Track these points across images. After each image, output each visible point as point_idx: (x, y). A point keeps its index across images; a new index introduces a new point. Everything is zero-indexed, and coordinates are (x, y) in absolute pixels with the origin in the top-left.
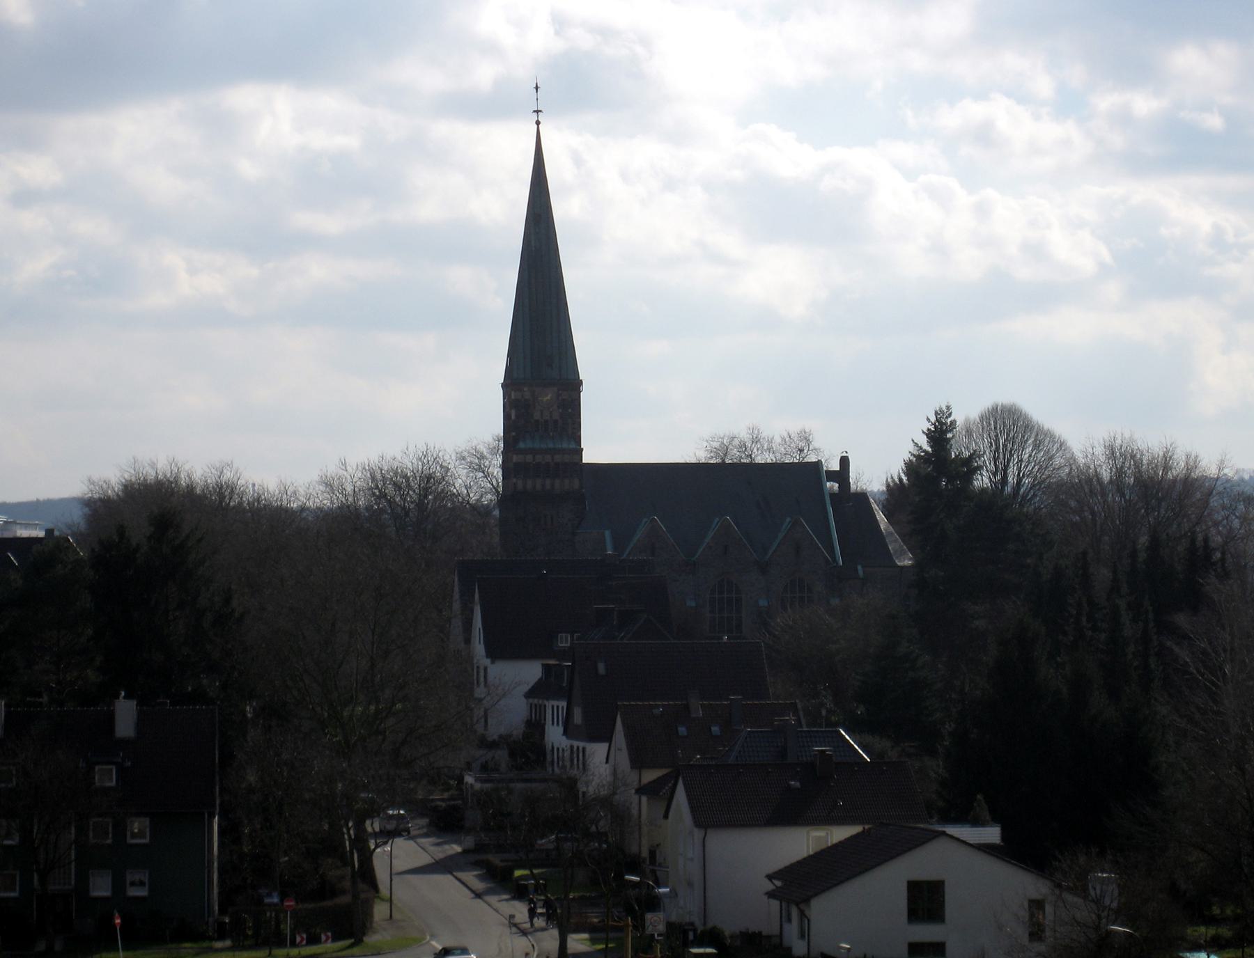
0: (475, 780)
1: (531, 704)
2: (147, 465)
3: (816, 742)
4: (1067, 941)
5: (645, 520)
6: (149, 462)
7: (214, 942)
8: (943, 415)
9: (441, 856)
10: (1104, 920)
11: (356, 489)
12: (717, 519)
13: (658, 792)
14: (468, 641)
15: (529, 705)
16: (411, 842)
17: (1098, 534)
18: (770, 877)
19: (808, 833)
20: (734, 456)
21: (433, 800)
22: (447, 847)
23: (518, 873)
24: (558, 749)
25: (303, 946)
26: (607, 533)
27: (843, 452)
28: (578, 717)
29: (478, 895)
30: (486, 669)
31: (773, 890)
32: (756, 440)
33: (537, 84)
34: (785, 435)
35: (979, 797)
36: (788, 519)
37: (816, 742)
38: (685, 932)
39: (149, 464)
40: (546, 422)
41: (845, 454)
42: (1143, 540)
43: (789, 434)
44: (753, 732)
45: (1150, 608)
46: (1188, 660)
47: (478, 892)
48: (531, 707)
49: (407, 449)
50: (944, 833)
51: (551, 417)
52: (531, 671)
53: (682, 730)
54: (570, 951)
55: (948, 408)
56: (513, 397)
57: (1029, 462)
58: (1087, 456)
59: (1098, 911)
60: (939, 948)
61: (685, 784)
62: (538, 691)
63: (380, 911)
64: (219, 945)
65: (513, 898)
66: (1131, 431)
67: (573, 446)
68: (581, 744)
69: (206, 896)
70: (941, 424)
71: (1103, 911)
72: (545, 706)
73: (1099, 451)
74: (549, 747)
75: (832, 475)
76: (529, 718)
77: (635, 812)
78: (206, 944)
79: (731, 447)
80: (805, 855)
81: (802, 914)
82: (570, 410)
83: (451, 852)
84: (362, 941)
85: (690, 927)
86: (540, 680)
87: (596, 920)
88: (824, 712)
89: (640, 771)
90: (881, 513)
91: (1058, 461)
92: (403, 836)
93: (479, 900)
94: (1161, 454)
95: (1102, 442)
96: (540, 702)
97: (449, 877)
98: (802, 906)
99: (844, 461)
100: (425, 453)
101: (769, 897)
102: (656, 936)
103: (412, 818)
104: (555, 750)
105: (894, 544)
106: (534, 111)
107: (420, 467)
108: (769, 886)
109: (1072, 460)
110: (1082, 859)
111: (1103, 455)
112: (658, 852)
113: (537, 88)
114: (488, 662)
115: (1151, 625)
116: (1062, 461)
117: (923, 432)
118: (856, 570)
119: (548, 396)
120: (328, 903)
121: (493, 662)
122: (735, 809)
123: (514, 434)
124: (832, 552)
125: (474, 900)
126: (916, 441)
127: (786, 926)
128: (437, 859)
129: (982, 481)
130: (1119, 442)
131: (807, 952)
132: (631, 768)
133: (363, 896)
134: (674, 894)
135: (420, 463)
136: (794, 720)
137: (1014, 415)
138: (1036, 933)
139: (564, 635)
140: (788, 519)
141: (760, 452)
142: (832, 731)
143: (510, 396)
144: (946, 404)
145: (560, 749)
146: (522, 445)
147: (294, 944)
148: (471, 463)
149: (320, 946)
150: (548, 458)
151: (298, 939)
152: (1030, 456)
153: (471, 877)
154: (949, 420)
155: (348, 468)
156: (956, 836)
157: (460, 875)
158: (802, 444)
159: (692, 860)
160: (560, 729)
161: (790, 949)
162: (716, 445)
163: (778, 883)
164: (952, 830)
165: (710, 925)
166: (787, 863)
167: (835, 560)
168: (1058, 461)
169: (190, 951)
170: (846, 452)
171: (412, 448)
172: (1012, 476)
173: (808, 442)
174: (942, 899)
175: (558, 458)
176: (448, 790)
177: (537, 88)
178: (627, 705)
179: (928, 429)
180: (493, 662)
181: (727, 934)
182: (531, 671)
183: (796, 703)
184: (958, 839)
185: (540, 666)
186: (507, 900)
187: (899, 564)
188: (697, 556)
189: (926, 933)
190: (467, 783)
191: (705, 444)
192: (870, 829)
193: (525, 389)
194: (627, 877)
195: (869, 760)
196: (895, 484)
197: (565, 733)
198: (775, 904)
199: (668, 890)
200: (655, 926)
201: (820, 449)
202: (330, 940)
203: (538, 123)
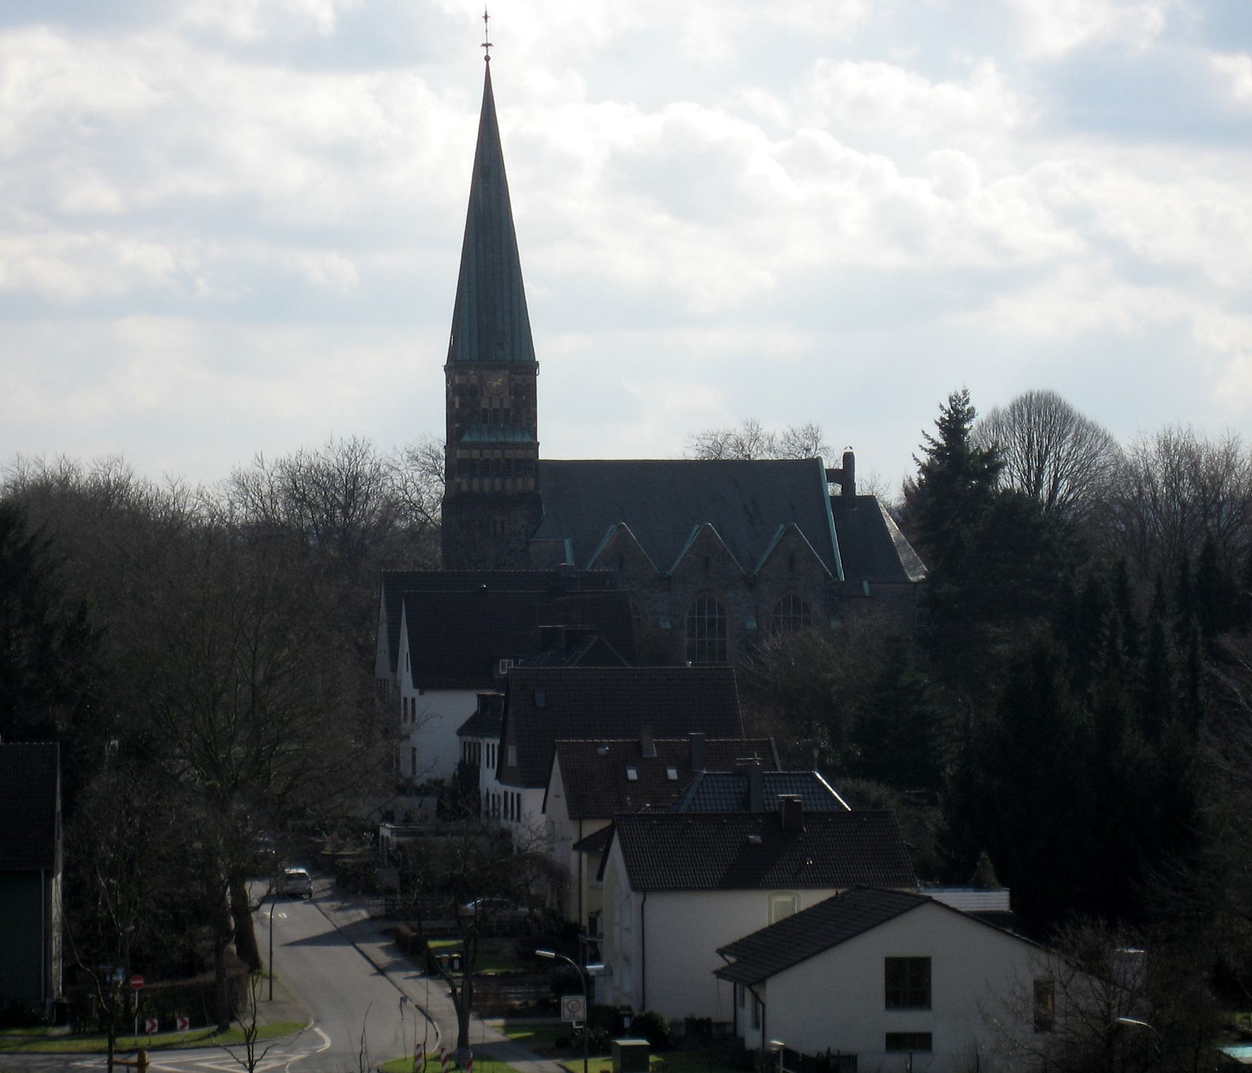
0: (392, 834)
1: (465, 743)
2: (32, 462)
3: (786, 787)
4: (1069, 1035)
5: (612, 527)
6: (36, 460)
7: (50, 1028)
8: (959, 401)
9: (344, 923)
10: (1115, 1010)
11: (275, 491)
12: (697, 526)
13: (595, 846)
14: (394, 668)
15: (463, 743)
16: (312, 907)
17: (1148, 545)
18: (722, 952)
19: (770, 900)
20: (730, 454)
21: (343, 856)
22: (352, 912)
23: (433, 944)
24: (493, 796)
25: (153, 1034)
26: (567, 542)
27: (846, 448)
28: (512, 758)
29: (381, 971)
30: (413, 700)
31: (724, 969)
32: (755, 438)
33: (486, 13)
34: (788, 431)
35: (984, 855)
36: (782, 526)
37: (786, 787)
38: (619, 1019)
39: (35, 462)
40: (496, 410)
41: (849, 450)
42: (1197, 552)
43: (792, 431)
44: (709, 775)
45: (1199, 629)
46: (1236, 690)
47: (381, 967)
48: (465, 747)
49: (331, 443)
50: (929, 899)
51: (502, 405)
52: (464, 705)
53: (632, 774)
54: (471, 1042)
55: (965, 393)
56: (457, 382)
57: (1067, 461)
58: (1138, 453)
59: (1108, 998)
60: (921, 1041)
61: (621, 839)
62: (471, 728)
63: (258, 990)
64: (57, 1031)
65: (423, 975)
66: (1189, 424)
67: (527, 439)
68: (516, 790)
69: (43, 972)
70: (957, 412)
71: (1114, 998)
72: (480, 744)
73: (1152, 447)
74: (483, 794)
75: (834, 475)
76: (462, 759)
77: (574, 872)
78: (37, 1031)
79: (726, 446)
80: (766, 925)
81: (756, 997)
82: (524, 398)
83: (358, 919)
84: (229, 1028)
85: (627, 1012)
86: (476, 714)
87: (517, 1003)
88: (816, 753)
89: (581, 824)
90: (891, 519)
91: (1102, 459)
92: (304, 899)
93: (381, 977)
94: (1222, 449)
95: (1155, 436)
96: (475, 740)
97: (352, 948)
98: (755, 988)
99: (849, 458)
100: (352, 447)
101: (718, 977)
102: (574, 1024)
103: (315, 879)
104: (491, 798)
105: (907, 555)
106: (483, 45)
107: (347, 464)
108: (720, 963)
109: (1118, 458)
110: (1087, 933)
111: (1156, 452)
112: (599, 919)
113: (486, 17)
114: (415, 693)
115: (1200, 650)
116: (1107, 458)
117: (936, 422)
118: (861, 586)
119: (497, 381)
120: (190, 981)
121: (421, 693)
122: (831, 857)
123: (457, 425)
124: (833, 566)
125: (376, 977)
126: (926, 433)
127: (740, 1011)
128: (338, 926)
129: (1009, 480)
130: (1175, 436)
131: (761, 1046)
132: (570, 818)
133: (231, 972)
134: (609, 971)
135: (346, 459)
136: (759, 761)
137: (1051, 404)
138: (1042, 1025)
139: (506, 661)
140: (782, 526)
141: (759, 452)
142: (807, 774)
143: (453, 381)
144: (962, 388)
145: (496, 796)
146: (466, 439)
147: (142, 1031)
148: (425, 463)
149: (175, 1034)
150: (498, 453)
151: (148, 1025)
152: (1069, 454)
153: (379, 950)
154: (967, 407)
155: (266, 465)
156: (944, 902)
157: (365, 946)
158: (807, 443)
159: (628, 930)
160: (493, 772)
161: (742, 1040)
162: (709, 443)
163: (732, 960)
164: (938, 895)
165: (649, 1009)
166: (736, 938)
167: (836, 574)
168: (1102, 459)
169: (19, 1039)
170: (851, 448)
171: (337, 442)
172: (1048, 478)
173: (816, 439)
174: (927, 980)
175: (510, 454)
176: (362, 844)
177: (486, 17)
178: (567, 743)
179: (942, 419)
180: (421, 693)
181: (667, 1021)
182: (464, 705)
183: (769, 742)
184: (947, 907)
185: (475, 696)
186: (415, 977)
187: (912, 579)
188: (672, 570)
189: (908, 1021)
190: (383, 836)
191: (696, 442)
192: (843, 893)
193: (472, 372)
194: (538, 952)
195: (850, 810)
196: (914, 487)
197: (499, 776)
198: (727, 986)
199: (602, 966)
200: (574, 1012)
201: (829, 448)
202: (187, 1027)
203: (487, 59)
